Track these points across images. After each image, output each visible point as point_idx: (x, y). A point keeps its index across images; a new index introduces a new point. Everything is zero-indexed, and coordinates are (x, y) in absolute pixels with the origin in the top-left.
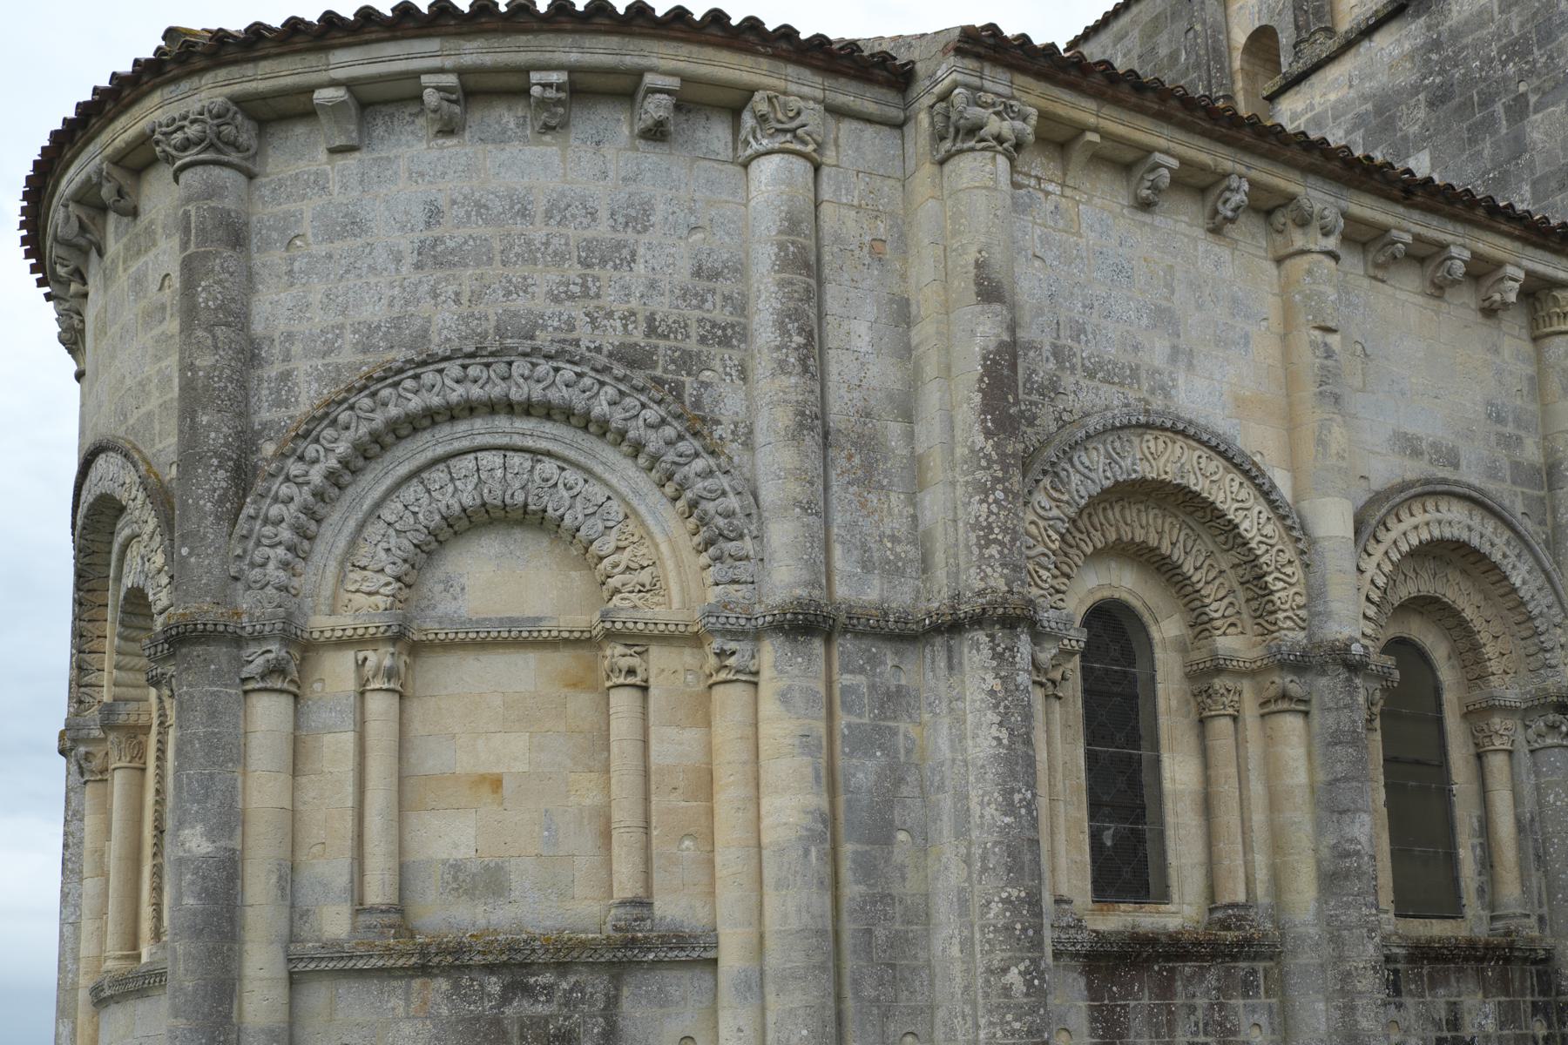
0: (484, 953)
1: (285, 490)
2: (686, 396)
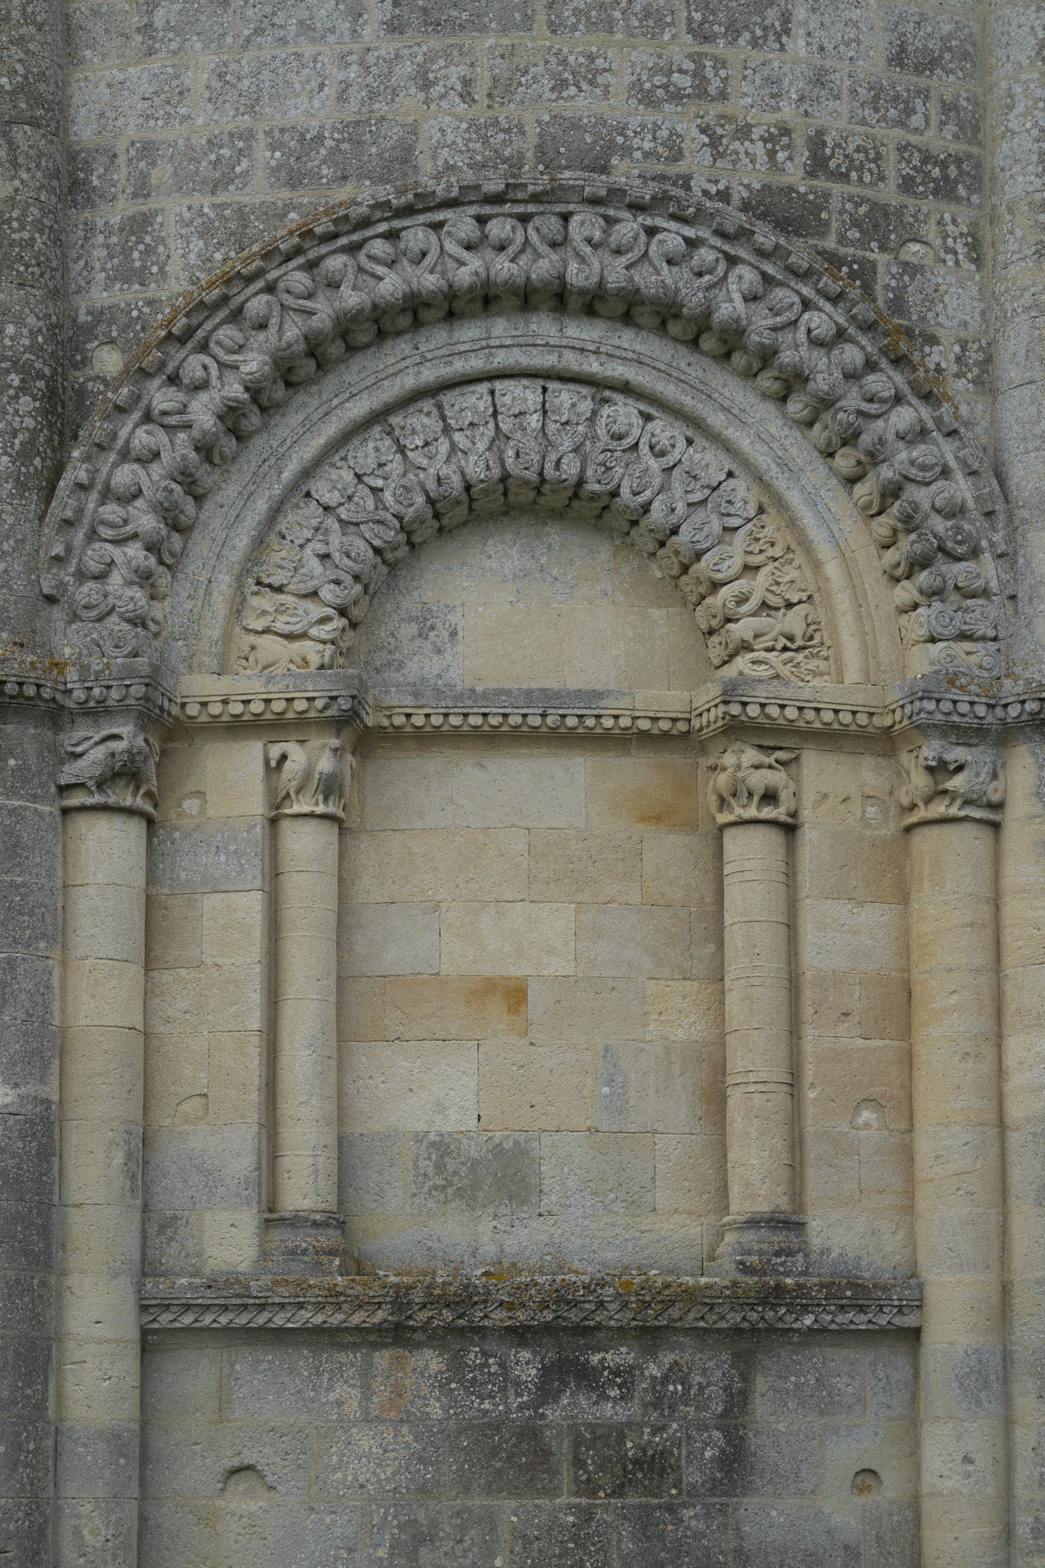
0: (511, 1307)
1: (143, 438)
2: (878, 288)
